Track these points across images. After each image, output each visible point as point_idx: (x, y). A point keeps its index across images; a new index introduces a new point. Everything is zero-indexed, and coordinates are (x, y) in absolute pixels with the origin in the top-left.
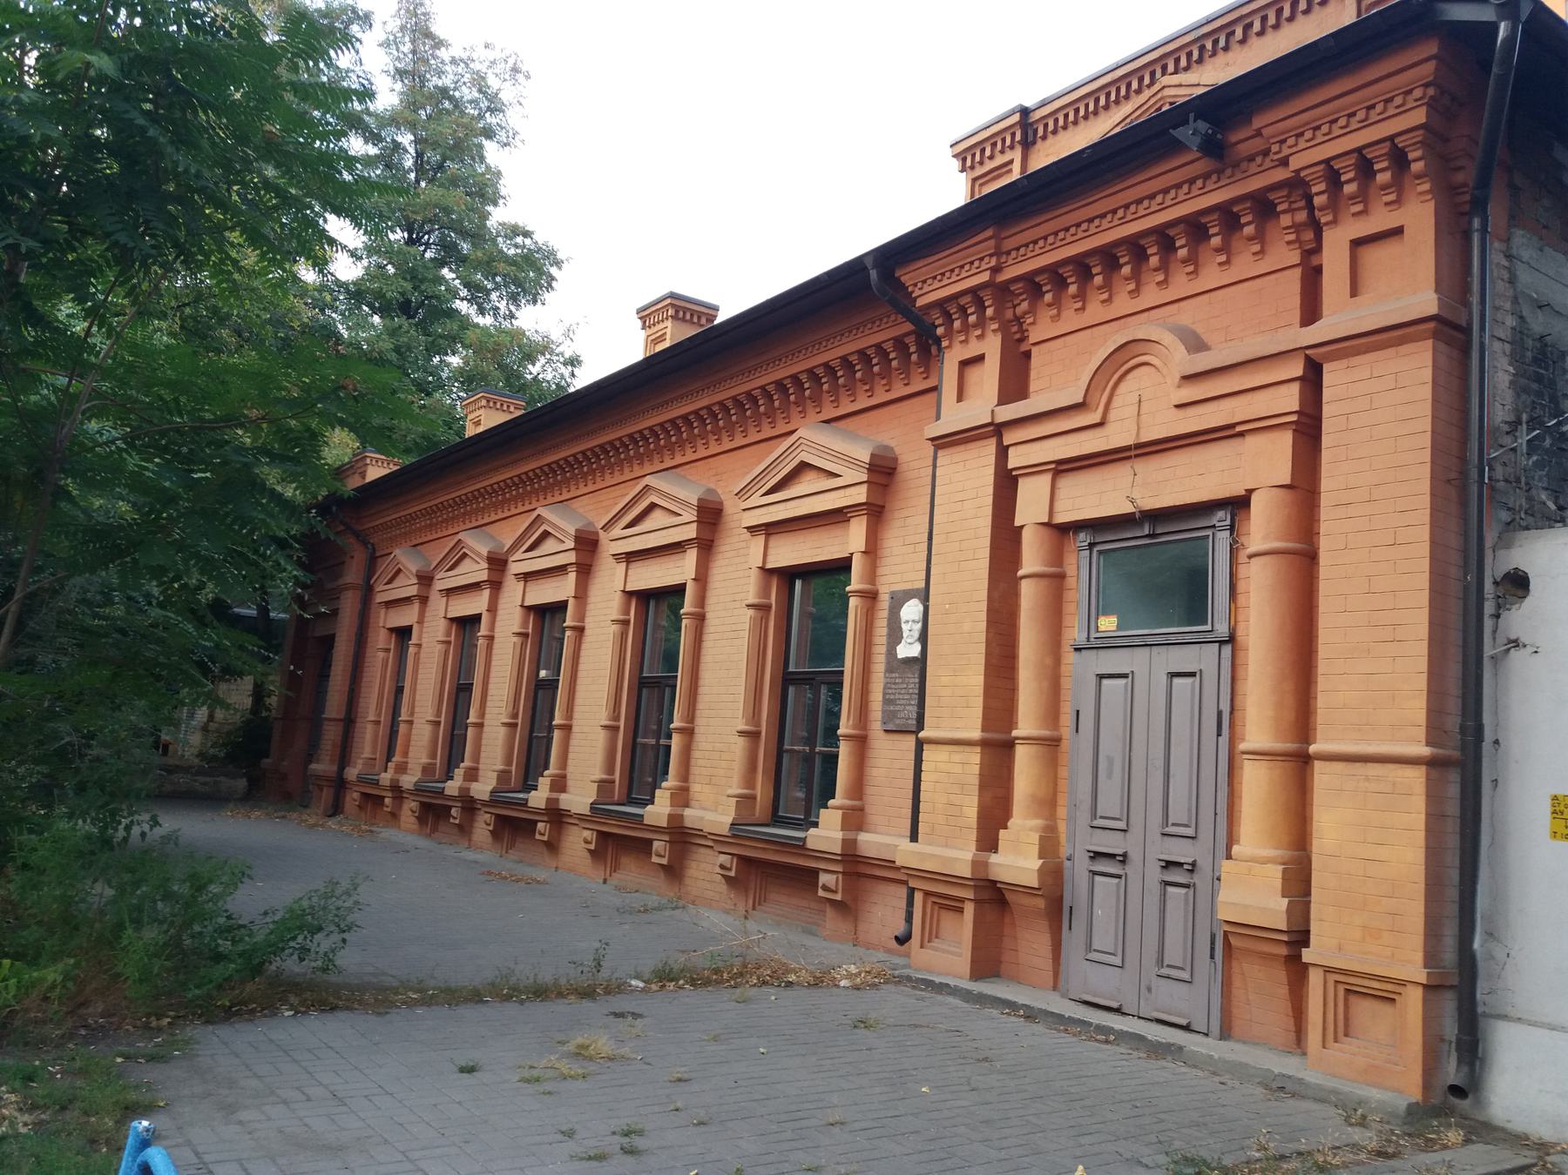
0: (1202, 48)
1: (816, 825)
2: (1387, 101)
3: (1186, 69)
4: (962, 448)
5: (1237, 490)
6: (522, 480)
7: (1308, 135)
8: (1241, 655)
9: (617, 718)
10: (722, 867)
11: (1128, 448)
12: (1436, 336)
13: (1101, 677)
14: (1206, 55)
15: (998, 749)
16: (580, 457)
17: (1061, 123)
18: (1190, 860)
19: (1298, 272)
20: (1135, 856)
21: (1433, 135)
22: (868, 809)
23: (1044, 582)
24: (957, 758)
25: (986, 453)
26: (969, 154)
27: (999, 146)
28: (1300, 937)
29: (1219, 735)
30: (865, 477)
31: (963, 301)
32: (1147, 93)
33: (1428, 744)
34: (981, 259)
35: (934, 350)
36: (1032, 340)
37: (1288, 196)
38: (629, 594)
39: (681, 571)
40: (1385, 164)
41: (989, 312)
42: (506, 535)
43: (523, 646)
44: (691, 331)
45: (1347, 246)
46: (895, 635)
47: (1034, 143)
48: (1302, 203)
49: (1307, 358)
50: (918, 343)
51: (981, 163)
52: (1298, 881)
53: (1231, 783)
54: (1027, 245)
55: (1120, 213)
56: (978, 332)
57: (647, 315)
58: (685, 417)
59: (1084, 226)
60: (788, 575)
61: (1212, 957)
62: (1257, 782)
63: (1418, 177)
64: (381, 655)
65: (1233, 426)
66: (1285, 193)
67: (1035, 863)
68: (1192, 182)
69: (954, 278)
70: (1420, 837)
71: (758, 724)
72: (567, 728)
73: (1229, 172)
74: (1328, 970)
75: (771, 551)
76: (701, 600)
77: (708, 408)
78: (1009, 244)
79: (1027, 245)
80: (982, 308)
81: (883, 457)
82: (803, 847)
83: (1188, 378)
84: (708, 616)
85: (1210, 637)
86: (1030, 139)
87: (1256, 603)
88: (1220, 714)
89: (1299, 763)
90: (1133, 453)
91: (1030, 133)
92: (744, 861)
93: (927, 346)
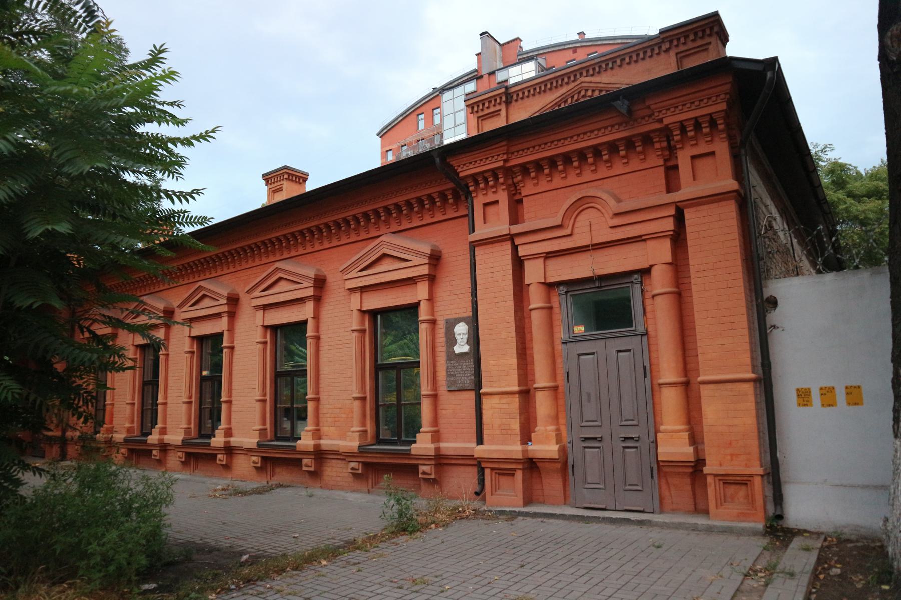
0: (600, 67)
2: (700, 101)
3: (592, 76)
4: (483, 247)
5: (645, 265)
7: (672, 110)
8: (652, 341)
9: (265, 395)
11: (588, 246)
13: (579, 355)
14: (602, 70)
15: (526, 395)
19: (662, 169)
20: (607, 438)
21: (727, 114)
22: (442, 431)
23: (544, 311)
24: (504, 401)
29: (645, 377)
30: (427, 262)
36: (523, 195)
38: (266, 328)
39: (221, 326)
41: (501, 181)
42: (174, 299)
43: (192, 358)
45: (481, 206)
46: (451, 341)
47: (511, 103)
50: (452, 194)
51: (482, 110)
52: (695, 439)
53: (653, 399)
55: (575, 138)
56: (494, 190)
59: (555, 143)
60: (373, 314)
61: (652, 477)
63: (721, 131)
65: (641, 237)
68: (612, 126)
71: (365, 393)
72: (229, 402)
73: (631, 123)
74: (716, 476)
75: (364, 301)
76: (317, 328)
78: (513, 149)
80: (496, 178)
81: (437, 252)
82: (410, 455)
83: (617, 215)
84: (322, 337)
87: (657, 316)
88: (645, 368)
89: (688, 387)
92: (366, 465)
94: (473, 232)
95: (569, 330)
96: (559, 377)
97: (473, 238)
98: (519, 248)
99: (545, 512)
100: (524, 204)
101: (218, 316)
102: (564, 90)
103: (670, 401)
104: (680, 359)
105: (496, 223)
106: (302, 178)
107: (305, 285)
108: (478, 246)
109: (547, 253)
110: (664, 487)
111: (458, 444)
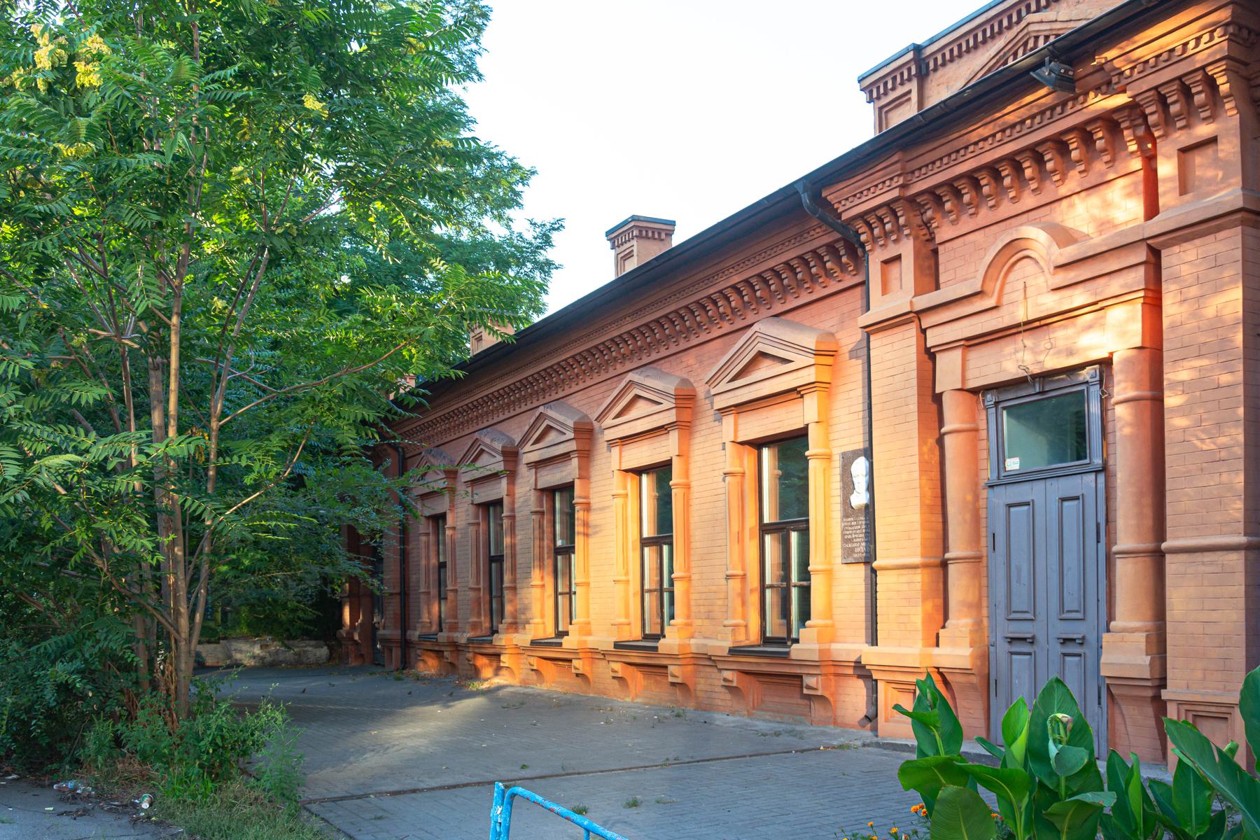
1: (797, 641)
4: (890, 332)
6: (511, 390)
10: (725, 680)
12: (1243, 222)
13: (1010, 506)
16: (570, 361)
17: (948, 57)
20: (1041, 638)
24: (903, 579)
26: (876, 86)
29: (1098, 542)
31: (880, 213)
32: (1016, 29)
34: (891, 179)
35: (860, 251)
37: (1129, 116)
40: (1200, 88)
44: (654, 250)
47: (927, 74)
48: (1140, 121)
49: (1149, 246)
54: (927, 166)
56: (1106, 158)
57: (617, 236)
58: (657, 321)
62: (1128, 574)
64: (424, 538)
69: (871, 196)
74: (1180, 703)
75: (740, 427)
77: (676, 311)
79: (927, 166)
84: (693, 484)
85: (1090, 468)
86: (924, 71)
90: (1021, 329)
91: (923, 67)
93: (856, 252)
94: (868, 309)
95: (1000, 462)
96: (983, 542)
101: (566, 456)
102: (1000, 43)
105: (895, 292)
106: (667, 228)
108: (1168, 245)
109: (967, 339)
111: (852, 646)
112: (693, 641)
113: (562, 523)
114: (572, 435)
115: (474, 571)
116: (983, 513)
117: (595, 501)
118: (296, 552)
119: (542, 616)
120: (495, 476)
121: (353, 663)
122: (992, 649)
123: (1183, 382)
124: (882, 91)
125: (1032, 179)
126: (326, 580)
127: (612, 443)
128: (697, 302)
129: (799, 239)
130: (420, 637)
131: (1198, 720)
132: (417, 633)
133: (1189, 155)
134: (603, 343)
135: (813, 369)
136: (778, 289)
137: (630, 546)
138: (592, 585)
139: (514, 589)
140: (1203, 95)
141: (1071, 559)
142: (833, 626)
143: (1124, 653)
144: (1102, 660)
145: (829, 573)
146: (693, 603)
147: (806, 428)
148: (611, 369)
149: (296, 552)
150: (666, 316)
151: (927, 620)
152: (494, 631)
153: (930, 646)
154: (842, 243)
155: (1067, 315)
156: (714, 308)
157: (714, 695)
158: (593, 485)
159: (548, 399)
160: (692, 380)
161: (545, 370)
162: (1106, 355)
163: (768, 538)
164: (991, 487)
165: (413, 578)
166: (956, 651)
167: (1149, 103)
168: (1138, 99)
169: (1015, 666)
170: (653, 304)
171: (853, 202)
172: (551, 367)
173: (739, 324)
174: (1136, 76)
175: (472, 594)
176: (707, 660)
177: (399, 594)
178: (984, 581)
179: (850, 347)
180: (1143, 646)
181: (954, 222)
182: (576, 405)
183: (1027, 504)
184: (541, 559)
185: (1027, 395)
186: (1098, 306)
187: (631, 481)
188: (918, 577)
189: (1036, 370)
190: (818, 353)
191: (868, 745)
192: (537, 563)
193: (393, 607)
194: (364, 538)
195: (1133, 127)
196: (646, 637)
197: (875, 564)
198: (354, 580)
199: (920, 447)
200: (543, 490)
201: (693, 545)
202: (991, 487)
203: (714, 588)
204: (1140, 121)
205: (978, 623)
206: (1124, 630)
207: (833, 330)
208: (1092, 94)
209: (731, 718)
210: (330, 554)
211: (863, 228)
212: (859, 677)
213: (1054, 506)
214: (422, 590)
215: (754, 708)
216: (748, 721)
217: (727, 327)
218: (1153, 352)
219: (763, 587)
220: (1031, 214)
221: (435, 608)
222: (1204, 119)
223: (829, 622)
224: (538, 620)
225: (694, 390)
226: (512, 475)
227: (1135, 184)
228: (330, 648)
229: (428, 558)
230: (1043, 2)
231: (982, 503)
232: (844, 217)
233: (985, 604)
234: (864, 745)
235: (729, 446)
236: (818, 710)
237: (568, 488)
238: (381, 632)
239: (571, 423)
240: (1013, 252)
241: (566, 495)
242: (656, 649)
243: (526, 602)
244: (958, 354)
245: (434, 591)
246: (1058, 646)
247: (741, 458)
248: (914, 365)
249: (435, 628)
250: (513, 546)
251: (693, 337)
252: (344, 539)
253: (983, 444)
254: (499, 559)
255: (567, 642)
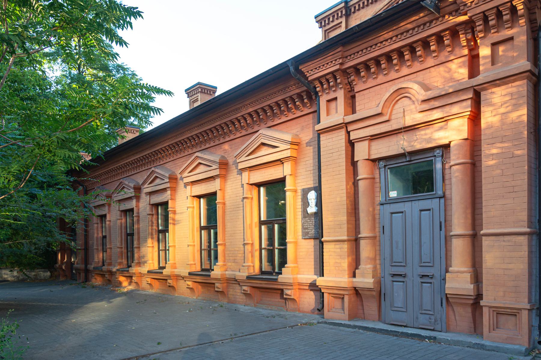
1: (213, 270)
4: (331, 133)
6: (138, 160)
8: (448, 202)
10: (244, 290)
13: (392, 213)
17: (361, 6)
18: (431, 274)
20: (409, 274)
24: (338, 246)
25: (341, 135)
26: (323, 20)
27: (336, 17)
28: (479, 296)
29: (441, 230)
31: (328, 77)
33: (528, 227)
34: (336, 60)
40: (507, 12)
42: (140, 179)
44: (208, 98)
46: (305, 203)
47: (350, 15)
48: (470, 31)
49: (474, 90)
50: (307, 95)
52: (477, 279)
53: (446, 247)
54: (354, 54)
56: (450, 49)
57: (189, 92)
58: (210, 129)
61: (442, 306)
64: (96, 225)
66: (463, 27)
67: (371, 280)
68: (424, 24)
70: (526, 260)
74: (490, 307)
75: (251, 177)
77: (220, 125)
79: (354, 54)
80: (336, 79)
84: (226, 203)
86: (348, 13)
88: (441, 223)
89: (475, 238)
90: (403, 130)
91: (348, 11)
95: (387, 193)
96: (377, 230)
97: (318, 127)
98: (351, 133)
99: (362, 325)
100: (356, 96)
101: (165, 190)
103: (459, 248)
104: (469, 216)
105: (334, 114)
106: (214, 89)
107: (214, 167)
108: (485, 89)
110: (451, 313)
112: (227, 272)
113: (161, 219)
114: (168, 180)
115: (120, 239)
116: (377, 217)
117: (178, 210)
118: (32, 230)
119: (153, 260)
120: (130, 198)
121: (62, 279)
122: (382, 279)
123: (493, 154)
124: (327, 22)
125: (408, 60)
126: (49, 244)
127: (186, 185)
128: (231, 121)
129: (284, 89)
130: (94, 268)
131: (499, 315)
132: (93, 266)
133: (496, 47)
134: (183, 140)
135: (289, 151)
136: (267, 116)
137: (195, 230)
138: (177, 247)
139: (139, 248)
140: (523, 10)
141: (426, 238)
142: (297, 267)
143: (459, 281)
144: (446, 286)
145: (296, 243)
146: (227, 255)
147: (285, 177)
148: (186, 152)
149: (32, 230)
150: (215, 127)
151: (349, 265)
152: (129, 266)
153: (351, 277)
154: (305, 93)
155: (428, 124)
156: (238, 124)
157: (237, 297)
158: (177, 203)
159: (155, 165)
160: (226, 156)
161: (155, 151)
162: (448, 143)
163: (263, 227)
164: (382, 204)
165: (91, 242)
166: (365, 279)
167: (479, 20)
168: (473, 18)
169: (395, 287)
170: (208, 122)
171: (314, 72)
172: (158, 150)
173: (250, 131)
174: (473, 6)
175: (119, 250)
176: (235, 281)
177: (84, 249)
178: (378, 248)
179: (307, 141)
180: (469, 280)
181: (365, 82)
182: (169, 168)
183: (402, 212)
184: (152, 234)
185: (401, 162)
186: (445, 120)
187: (196, 201)
188: (345, 246)
189: (409, 149)
190: (292, 143)
191: (321, 323)
192: (150, 236)
193: (81, 254)
194: (68, 223)
195: (466, 34)
196: (203, 270)
197: (323, 239)
198: (63, 244)
199: (346, 185)
200: (153, 205)
201: (227, 230)
202: (382, 204)
203: (237, 249)
204: (470, 31)
205: (375, 268)
206: (458, 272)
207: (298, 133)
208: (447, 17)
209: (247, 308)
210: (50, 232)
211: (318, 84)
212: (311, 290)
213: (388, 215)
214: (95, 247)
215: (257, 303)
216: (255, 309)
217: (244, 133)
218: (474, 141)
219: (261, 249)
220: (406, 77)
221: (101, 255)
222: (507, 28)
223: (296, 265)
224: (151, 262)
225: (227, 161)
226: (138, 198)
227: (463, 62)
228: (51, 272)
229: (98, 233)
230: (370, 1)
231: (377, 212)
232: (310, 79)
233: (378, 258)
234: (318, 323)
235: (246, 186)
236: (290, 305)
237: (165, 204)
238: (75, 265)
239: (167, 175)
240: (400, 94)
241: (131, 213)
242: (210, 276)
243: (145, 253)
244: (366, 143)
245: (100, 248)
246: (419, 278)
247: (251, 191)
248: (344, 148)
249: (101, 264)
250: (138, 229)
251: (227, 137)
252: (58, 224)
253: (378, 185)
254: (132, 235)
255: (165, 272)
